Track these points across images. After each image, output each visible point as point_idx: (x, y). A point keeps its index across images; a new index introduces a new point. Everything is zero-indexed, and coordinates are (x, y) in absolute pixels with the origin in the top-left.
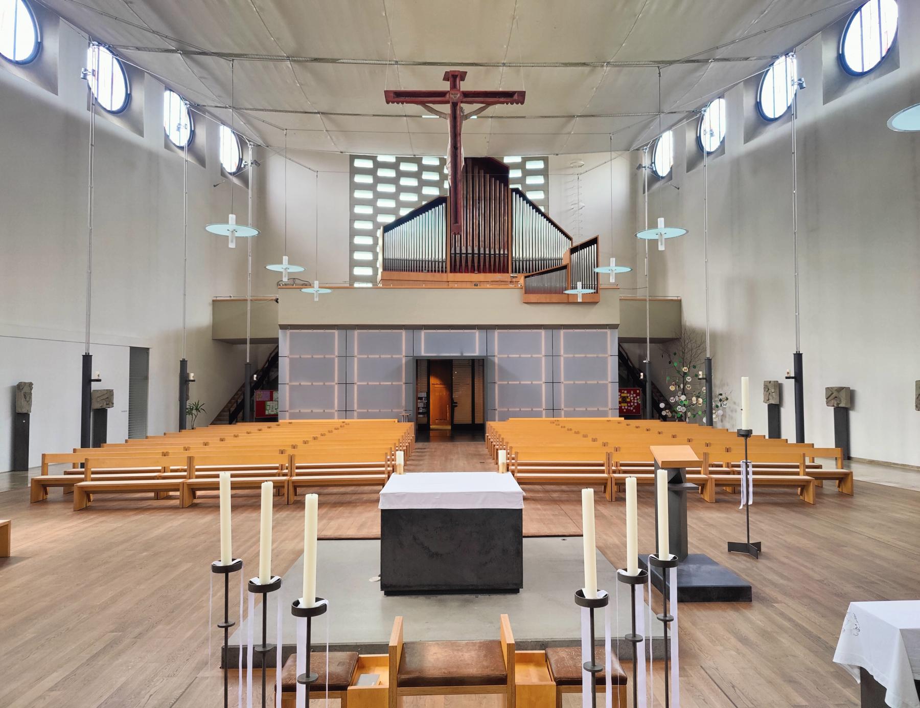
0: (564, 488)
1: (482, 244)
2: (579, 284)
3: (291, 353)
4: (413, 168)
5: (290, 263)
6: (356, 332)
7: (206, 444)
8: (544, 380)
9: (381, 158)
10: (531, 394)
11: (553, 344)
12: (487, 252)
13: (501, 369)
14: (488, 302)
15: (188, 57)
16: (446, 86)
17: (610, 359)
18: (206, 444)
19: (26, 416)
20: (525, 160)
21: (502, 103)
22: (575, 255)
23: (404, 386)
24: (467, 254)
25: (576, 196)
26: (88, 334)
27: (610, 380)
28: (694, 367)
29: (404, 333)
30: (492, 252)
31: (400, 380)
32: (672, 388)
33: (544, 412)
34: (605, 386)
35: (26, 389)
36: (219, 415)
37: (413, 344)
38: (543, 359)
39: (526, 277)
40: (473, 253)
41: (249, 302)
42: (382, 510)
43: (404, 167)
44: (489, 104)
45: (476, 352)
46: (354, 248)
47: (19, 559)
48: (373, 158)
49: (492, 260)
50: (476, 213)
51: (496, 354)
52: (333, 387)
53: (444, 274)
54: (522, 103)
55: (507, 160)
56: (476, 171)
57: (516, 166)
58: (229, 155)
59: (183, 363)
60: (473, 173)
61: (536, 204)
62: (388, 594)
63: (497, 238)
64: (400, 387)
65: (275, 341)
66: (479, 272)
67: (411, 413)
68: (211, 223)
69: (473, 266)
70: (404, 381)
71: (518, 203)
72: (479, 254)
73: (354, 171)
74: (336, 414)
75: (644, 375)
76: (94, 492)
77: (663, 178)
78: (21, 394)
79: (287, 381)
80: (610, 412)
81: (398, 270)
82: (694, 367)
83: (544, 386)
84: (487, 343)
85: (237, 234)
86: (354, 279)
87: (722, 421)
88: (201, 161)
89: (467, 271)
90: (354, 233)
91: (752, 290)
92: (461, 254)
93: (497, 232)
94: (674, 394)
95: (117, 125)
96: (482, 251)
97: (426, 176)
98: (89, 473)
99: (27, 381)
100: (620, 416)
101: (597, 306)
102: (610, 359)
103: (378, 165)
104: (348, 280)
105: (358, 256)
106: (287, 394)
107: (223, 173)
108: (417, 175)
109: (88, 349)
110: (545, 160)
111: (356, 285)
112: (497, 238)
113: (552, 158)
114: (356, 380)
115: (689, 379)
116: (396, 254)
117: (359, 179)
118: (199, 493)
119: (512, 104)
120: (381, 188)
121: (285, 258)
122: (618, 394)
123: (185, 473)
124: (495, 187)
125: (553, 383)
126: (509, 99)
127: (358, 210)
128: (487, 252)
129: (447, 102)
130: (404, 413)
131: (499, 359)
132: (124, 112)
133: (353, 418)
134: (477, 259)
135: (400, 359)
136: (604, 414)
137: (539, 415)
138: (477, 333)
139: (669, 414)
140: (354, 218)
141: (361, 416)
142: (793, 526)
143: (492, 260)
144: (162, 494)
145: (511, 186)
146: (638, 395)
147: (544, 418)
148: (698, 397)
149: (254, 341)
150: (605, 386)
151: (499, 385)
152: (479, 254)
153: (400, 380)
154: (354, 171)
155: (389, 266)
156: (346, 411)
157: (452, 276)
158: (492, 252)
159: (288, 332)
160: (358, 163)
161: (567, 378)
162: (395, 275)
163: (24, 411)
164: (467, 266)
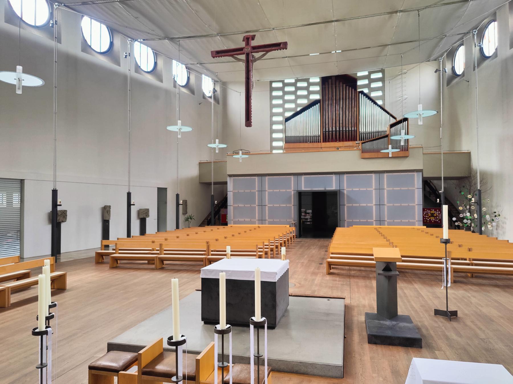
0: (362, 268)
1: (341, 125)
2: (390, 146)
3: (234, 190)
4: (305, 84)
6: (267, 178)
7: (178, 237)
8: (374, 203)
9: (286, 81)
10: (366, 213)
12: (344, 129)
14: (344, 158)
15: (173, 42)
16: (243, 44)
17: (232, 204)
18: (178, 237)
19: (108, 221)
20: (370, 73)
21: (275, 50)
22: (393, 128)
23: (293, 207)
24: (332, 131)
25: (406, 93)
26: (129, 181)
29: (292, 177)
31: (290, 203)
32: (461, 208)
35: (108, 209)
36: (204, 221)
37: (298, 183)
38: (374, 191)
39: (362, 143)
40: (336, 131)
41: (213, 164)
42: (202, 279)
43: (299, 84)
44: (268, 52)
45: (333, 187)
46: (272, 131)
47: (70, 290)
48: (283, 81)
49: (347, 134)
50: (337, 108)
51: (345, 188)
52: (255, 207)
53: (319, 144)
54: (286, 49)
56: (338, 83)
57: (363, 78)
58: (207, 86)
59: (177, 196)
60: (336, 84)
61: (374, 99)
62: (206, 323)
63: (350, 121)
64: (290, 207)
65: (226, 183)
66: (340, 141)
67: (297, 222)
68: (170, 125)
69: (336, 138)
70: (293, 204)
71: (363, 100)
72: (339, 131)
73: (272, 89)
75: (440, 201)
76: (120, 260)
77: (458, 76)
78: (106, 211)
79: (232, 204)
80: (417, 223)
81: (293, 142)
84: (340, 182)
85: (182, 131)
86: (273, 148)
87: (497, 229)
88: (192, 92)
89: (332, 141)
92: (329, 131)
93: (350, 118)
94: (463, 212)
95: (150, 79)
96: (341, 129)
98: (117, 250)
99: (108, 205)
100: (423, 225)
101: (408, 159)
102: (416, 191)
103: (285, 85)
104: (269, 149)
105: (275, 135)
106: (232, 211)
107: (204, 97)
108: (307, 88)
109: (129, 189)
110: (382, 71)
111: (274, 151)
112: (350, 121)
113: (387, 71)
116: (292, 133)
118: (165, 262)
119: (280, 50)
120: (287, 97)
123: (158, 252)
124: (349, 91)
125: (380, 205)
126: (278, 47)
128: (344, 129)
129: (243, 54)
131: (347, 191)
132: (154, 72)
133: (385, 225)
134: (339, 133)
135: (291, 192)
136: (413, 224)
137: (371, 224)
138: (334, 176)
139: (461, 225)
140: (272, 115)
141: (270, 223)
142: (496, 301)
143: (347, 134)
144: (151, 262)
145: (359, 90)
149: (215, 183)
150: (414, 206)
151: (347, 206)
152: (339, 131)
154: (272, 89)
155: (288, 140)
156: (262, 221)
157: (324, 144)
158: (347, 129)
159: (232, 178)
160: (274, 85)
162: (292, 145)
163: (107, 219)
164: (332, 138)
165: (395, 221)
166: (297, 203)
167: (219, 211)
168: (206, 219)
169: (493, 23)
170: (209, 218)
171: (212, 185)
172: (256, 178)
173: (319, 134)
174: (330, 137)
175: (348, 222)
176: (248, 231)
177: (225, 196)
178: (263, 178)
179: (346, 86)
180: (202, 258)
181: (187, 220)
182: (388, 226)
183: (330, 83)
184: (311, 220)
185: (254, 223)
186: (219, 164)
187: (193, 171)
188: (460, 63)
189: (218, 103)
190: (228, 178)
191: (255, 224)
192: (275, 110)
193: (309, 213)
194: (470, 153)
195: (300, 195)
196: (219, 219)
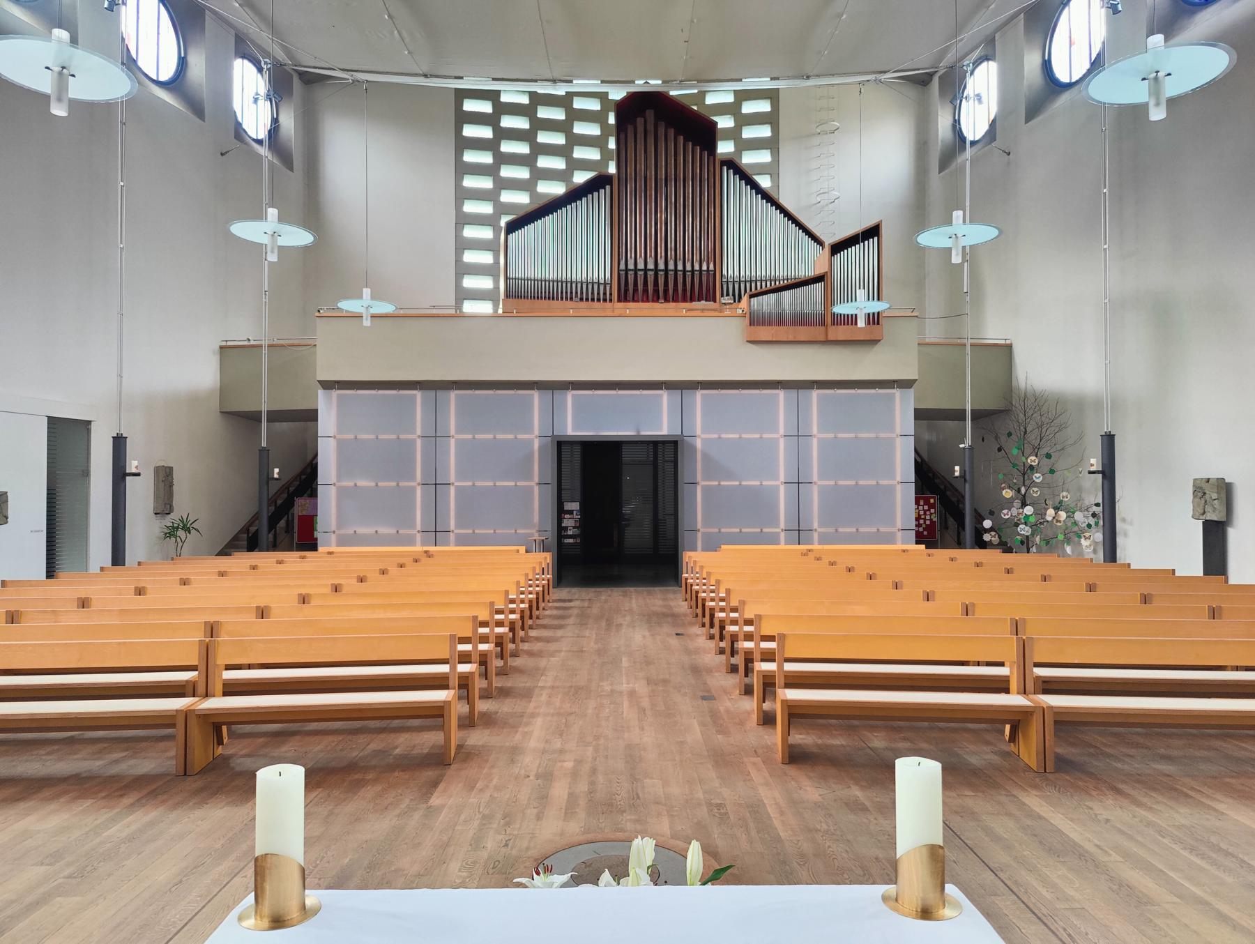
3: (339, 430)
5: (373, 297)
11: (799, 414)
12: (680, 267)
13: (706, 457)
17: (333, 479)
23: (536, 489)
24: (646, 270)
27: (899, 479)
28: (1048, 456)
30: (689, 267)
31: (529, 477)
33: (782, 535)
34: (890, 490)
36: (236, 538)
37: (553, 412)
40: (656, 270)
41: (265, 351)
45: (663, 428)
51: (698, 432)
52: (413, 489)
53: (608, 304)
55: (718, 96)
56: (661, 131)
67: (551, 536)
69: (656, 291)
70: (536, 479)
72: (666, 270)
74: (419, 537)
79: (333, 479)
80: (899, 534)
81: (526, 296)
82: (1048, 456)
83: (782, 488)
84: (683, 412)
85: (281, 242)
88: (197, 109)
90: (463, 245)
91: (1163, 315)
94: (1009, 504)
97: (580, 128)
101: (877, 348)
102: (899, 441)
105: (469, 282)
107: (239, 132)
114: (452, 478)
115: (1038, 478)
117: (470, 157)
120: (507, 172)
121: (367, 292)
122: (914, 506)
125: (798, 483)
127: (470, 207)
128: (680, 267)
130: (536, 537)
131: (704, 441)
133: (448, 545)
135: (531, 442)
136: (889, 539)
137: (773, 540)
141: (462, 540)
146: (932, 506)
147: (782, 546)
148: (1057, 509)
149: (275, 416)
152: (666, 270)
153: (530, 478)
158: (689, 267)
159: (335, 393)
161: (822, 475)
165: (841, 530)
166: (551, 476)
167: (289, 504)
168: (245, 530)
169: (985, 64)
170: (253, 529)
171: (264, 425)
172: (418, 394)
173: (608, 275)
174: (640, 287)
175: (707, 537)
176: (394, 571)
177: (309, 458)
178: (440, 393)
179: (686, 141)
180: (165, 720)
181: (171, 532)
182: (820, 547)
183: (640, 129)
184: (577, 531)
185: (410, 541)
186: (288, 355)
187: (201, 374)
188: (982, 100)
189: (290, 167)
190: (321, 392)
191: (894, 543)
192: (470, 207)
193: (571, 512)
194: (1010, 346)
195: (562, 446)
196: (289, 529)
